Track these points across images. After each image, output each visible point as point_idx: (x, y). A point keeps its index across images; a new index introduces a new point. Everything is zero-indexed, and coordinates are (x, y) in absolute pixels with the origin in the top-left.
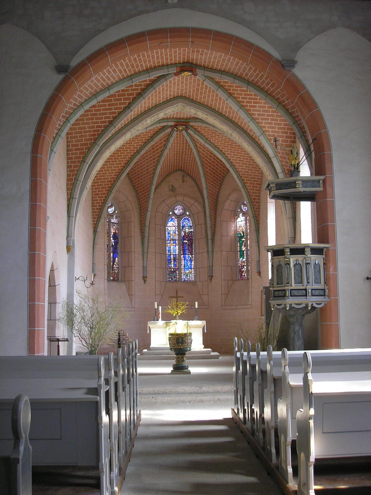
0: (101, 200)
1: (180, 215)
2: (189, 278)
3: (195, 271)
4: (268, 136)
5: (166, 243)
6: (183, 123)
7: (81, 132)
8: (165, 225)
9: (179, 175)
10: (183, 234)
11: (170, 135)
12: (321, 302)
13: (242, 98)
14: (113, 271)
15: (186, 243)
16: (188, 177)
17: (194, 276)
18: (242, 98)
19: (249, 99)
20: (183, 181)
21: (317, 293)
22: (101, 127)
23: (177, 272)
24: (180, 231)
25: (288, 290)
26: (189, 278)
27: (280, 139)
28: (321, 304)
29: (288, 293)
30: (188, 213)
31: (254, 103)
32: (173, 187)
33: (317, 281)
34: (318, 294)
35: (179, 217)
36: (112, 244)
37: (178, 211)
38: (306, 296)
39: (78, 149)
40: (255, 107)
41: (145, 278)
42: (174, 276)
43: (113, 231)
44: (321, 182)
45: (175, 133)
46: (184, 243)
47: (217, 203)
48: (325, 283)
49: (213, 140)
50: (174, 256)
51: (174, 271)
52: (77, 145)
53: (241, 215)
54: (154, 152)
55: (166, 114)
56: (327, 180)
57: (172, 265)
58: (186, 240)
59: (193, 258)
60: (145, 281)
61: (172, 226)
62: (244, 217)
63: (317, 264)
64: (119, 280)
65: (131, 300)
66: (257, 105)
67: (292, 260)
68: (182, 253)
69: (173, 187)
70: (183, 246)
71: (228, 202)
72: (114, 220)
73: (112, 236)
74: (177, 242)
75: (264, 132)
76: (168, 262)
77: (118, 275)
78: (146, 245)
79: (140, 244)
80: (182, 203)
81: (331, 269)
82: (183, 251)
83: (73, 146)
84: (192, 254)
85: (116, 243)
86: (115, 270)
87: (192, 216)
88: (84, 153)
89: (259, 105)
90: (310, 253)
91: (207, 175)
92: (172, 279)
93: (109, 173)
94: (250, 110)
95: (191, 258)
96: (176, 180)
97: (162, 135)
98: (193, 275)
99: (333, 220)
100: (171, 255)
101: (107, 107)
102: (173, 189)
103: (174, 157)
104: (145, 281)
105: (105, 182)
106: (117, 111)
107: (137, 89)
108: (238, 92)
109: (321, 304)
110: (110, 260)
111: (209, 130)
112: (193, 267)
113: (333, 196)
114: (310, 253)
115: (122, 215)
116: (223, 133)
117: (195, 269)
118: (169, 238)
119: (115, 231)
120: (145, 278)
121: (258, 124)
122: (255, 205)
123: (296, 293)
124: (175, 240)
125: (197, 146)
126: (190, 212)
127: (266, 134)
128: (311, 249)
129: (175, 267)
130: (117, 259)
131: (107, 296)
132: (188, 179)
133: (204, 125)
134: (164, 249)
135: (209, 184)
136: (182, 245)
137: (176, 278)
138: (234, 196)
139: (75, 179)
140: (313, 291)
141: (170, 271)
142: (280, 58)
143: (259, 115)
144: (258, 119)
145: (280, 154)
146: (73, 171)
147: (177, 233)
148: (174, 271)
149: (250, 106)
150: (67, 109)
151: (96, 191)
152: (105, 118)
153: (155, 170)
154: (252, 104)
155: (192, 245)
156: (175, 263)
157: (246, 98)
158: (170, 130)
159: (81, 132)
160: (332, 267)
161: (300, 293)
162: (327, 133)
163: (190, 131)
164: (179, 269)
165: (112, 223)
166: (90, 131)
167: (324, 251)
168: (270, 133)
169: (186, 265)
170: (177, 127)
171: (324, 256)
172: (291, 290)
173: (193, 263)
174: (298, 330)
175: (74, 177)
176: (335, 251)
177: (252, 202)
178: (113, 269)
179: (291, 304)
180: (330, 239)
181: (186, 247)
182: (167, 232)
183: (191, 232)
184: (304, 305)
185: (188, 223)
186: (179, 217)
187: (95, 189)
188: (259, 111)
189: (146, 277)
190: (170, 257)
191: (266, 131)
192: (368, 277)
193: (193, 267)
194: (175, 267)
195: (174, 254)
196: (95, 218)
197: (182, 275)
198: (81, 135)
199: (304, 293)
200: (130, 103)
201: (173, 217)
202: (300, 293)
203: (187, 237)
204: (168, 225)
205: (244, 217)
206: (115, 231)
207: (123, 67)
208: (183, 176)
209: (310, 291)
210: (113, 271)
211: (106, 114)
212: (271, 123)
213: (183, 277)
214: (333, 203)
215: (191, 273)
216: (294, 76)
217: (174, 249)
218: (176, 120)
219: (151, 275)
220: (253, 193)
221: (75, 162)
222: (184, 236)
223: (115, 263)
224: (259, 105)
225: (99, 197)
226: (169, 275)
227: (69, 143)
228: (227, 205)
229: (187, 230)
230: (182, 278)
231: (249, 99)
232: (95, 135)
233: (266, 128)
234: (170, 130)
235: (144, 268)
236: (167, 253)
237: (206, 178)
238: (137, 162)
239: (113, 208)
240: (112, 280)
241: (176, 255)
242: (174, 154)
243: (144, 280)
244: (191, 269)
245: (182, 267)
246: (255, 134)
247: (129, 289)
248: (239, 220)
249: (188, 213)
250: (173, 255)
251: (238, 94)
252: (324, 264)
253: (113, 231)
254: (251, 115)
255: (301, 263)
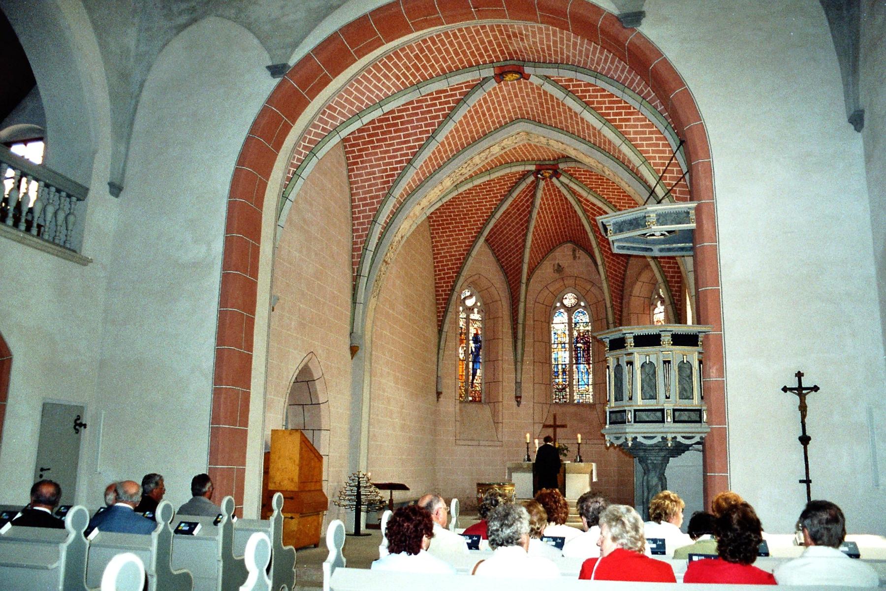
0: (447, 286)
1: (572, 307)
2: (584, 398)
3: (594, 388)
4: (654, 166)
5: (550, 348)
6: (548, 167)
7: (370, 180)
8: (549, 321)
9: (567, 248)
10: (575, 334)
11: (535, 186)
12: (654, 433)
13: (607, 108)
14: (472, 388)
15: (581, 347)
16: (581, 251)
17: (592, 395)
18: (607, 108)
19: (618, 108)
20: (575, 258)
21: (685, 416)
22: (396, 169)
23: (568, 390)
24: (571, 330)
25: (631, 411)
26: (584, 398)
27: (675, 169)
28: (656, 437)
29: (630, 416)
30: (582, 304)
31: (626, 114)
32: (558, 265)
33: (685, 393)
34: (686, 419)
35: (570, 310)
36: (472, 350)
37: (570, 300)
38: (664, 422)
39: (367, 205)
40: (628, 120)
41: (518, 398)
42: (563, 396)
43: (472, 331)
44: (692, 212)
45: (542, 184)
46: (578, 347)
47: (623, 287)
48: (702, 398)
49: (600, 191)
50: (564, 367)
51: (564, 389)
52: (365, 199)
53: (659, 303)
54: (520, 214)
55: (504, 148)
56: (705, 210)
57: (561, 380)
58: (580, 343)
59: (591, 369)
60: (519, 403)
61: (560, 322)
62: (663, 307)
63: (685, 362)
64: (482, 402)
65: (497, 429)
66: (632, 117)
67: (639, 356)
68: (574, 362)
69: (560, 266)
70: (574, 350)
71: (639, 284)
72: (475, 316)
73: (471, 338)
74: (567, 346)
75: (646, 161)
76: (555, 376)
77: (480, 394)
78: (519, 351)
79: (511, 348)
80: (575, 289)
81: (713, 372)
82: (575, 359)
83: (361, 200)
84: (589, 364)
85: (478, 349)
86: (476, 386)
87: (588, 307)
88: (375, 209)
89: (634, 117)
90: (672, 342)
91: (602, 245)
92: (560, 400)
93: (456, 247)
94: (621, 126)
95: (587, 370)
96: (563, 254)
97: (523, 186)
98: (591, 394)
99: (716, 281)
100: (558, 365)
101: (403, 140)
102: (559, 269)
103: (554, 221)
104: (519, 403)
105: (451, 260)
106: (417, 144)
107: (444, 109)
108: (599, 99)
109: (656, 437)
110: (469, 372)
111: (593, 175)
112: (590, 383)
113: (714, 237)
114: (672, 342)
115: (487, 310)
116: (589, 169)
117: (594, 384)
118: (556, 340)
119: (477, 331)
120: (518, 398)
121: (636, 148)
122: (674, 287)
123: (644, 416)
124: (564, 343)
125: (581, 202)
126: (586, 301)
127: (650, 163)
128: (672, 335)
129: (564, 383)
130: (478, 371)
131: (458, 424)
132: (581, 253)
133: (573, 165)
134: (548, 355)
135: (606, 259)
136: (575, 351)
137: (566, 398)
138: (645, 277)
139: (363, 248)
140: (677, 414)
141: (557, 389)
142: (616, 12)
143: (635, 133)
144: (636, 139)
145: (676, 194)
146: (360, 236)
147: (567, 332)
148: (564, 389)
149: (621, 120)
150: (310, 135)
151: (440, 275)
152: (402, 155)
153: (524, 241)
154: (623, 117)
155: (588, 350)
156: (565, 377)
157: (612, 108)
158: (532, 178)
159: (370, 180)
160: (715, 368)
161: (652, 416)
162: (702, 129)
163: (562, 178)
164: (571, 385)
165: (472, 320)
166: (382, 177)
167: (700, 339)
168: (657, 161)
169: (580, 380)
170: (541, 173)
171: (699, 349)
172: (635, 411)
173: (591, 376)
174: (657, 485)
175: (362, 246)
176: (720, 339)
177: (667, 281)
178: (472, 385)
179: (636, 438)
180: (711, 319)
181: (580, 353)
182: (552, 332)
183: (588, 331)
184: (659, 439)
185: (583, 319)
186: (570, 310)
187: (439, 271)
188: (636, 126)
189: (520, 397)
190: (557, 368)
191: (650, 158)
192: (785, 387)
193: (590, 383)
194: (564, 383)
195: (563, 363)
196: (440, 312)
197: (575, 394)
198: (370, 184)
199: (659, 416)
200: (434, 131)
201: (562, 310)
202: (652, 416)
203: (582, 339)
204: (554, 322)
205: (663, 307)
206: (477, 331)
207: (399, 69)
208: (574, 251)
209: (670, 412)
210: (472, 388)
211: (402, 149)
212: (658, 145)
213: (576, 397)
214: (715, 250)
215: (587, 392)
216: (640, 35)
217: (562, 356)
218: (538, 163)
219: (527, 394)
220: (669, 267)
221: (363, 224)
222: (577, 338)
223: (476, 377)
224: (634, 117)
225: (444, 283)
226: (556, 395)
227: (354, 196)
228: (639, 290)
229: (582, 328)
230: (575, 398)
231: (618, 108)
232: (388, 182)
233: (649, 153)
234: (532, 178)
235: (518, 384)
236: (553, 362)
237: (601, 249)
238: (492, 229)
239: (474, 298)
240: (471, 401)
241: (565, 364)
242: (552, 217)
243: (517, 401)
244: (588, 385)
245: (574, 383)
246: (632, 164)
247: (495, 413)
248: (656, 311)
249: (582, 304)
250: (562, 365)
251: (598, 102)
252: (700, 362)
253: (472, 331)
254: (623, 134)
255: (654, 362)
